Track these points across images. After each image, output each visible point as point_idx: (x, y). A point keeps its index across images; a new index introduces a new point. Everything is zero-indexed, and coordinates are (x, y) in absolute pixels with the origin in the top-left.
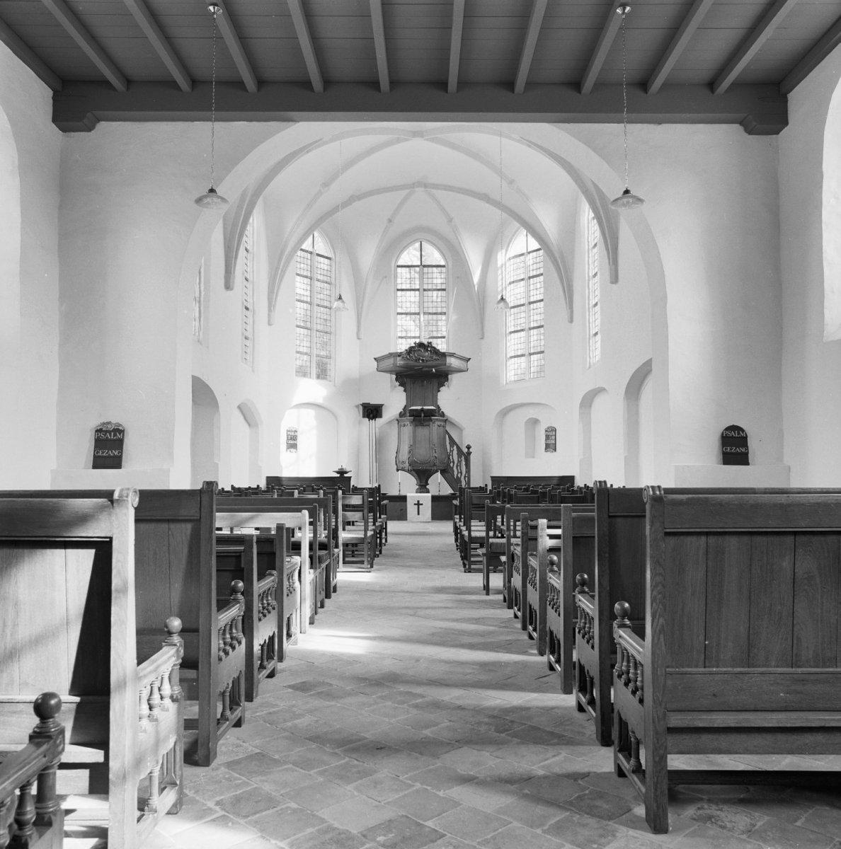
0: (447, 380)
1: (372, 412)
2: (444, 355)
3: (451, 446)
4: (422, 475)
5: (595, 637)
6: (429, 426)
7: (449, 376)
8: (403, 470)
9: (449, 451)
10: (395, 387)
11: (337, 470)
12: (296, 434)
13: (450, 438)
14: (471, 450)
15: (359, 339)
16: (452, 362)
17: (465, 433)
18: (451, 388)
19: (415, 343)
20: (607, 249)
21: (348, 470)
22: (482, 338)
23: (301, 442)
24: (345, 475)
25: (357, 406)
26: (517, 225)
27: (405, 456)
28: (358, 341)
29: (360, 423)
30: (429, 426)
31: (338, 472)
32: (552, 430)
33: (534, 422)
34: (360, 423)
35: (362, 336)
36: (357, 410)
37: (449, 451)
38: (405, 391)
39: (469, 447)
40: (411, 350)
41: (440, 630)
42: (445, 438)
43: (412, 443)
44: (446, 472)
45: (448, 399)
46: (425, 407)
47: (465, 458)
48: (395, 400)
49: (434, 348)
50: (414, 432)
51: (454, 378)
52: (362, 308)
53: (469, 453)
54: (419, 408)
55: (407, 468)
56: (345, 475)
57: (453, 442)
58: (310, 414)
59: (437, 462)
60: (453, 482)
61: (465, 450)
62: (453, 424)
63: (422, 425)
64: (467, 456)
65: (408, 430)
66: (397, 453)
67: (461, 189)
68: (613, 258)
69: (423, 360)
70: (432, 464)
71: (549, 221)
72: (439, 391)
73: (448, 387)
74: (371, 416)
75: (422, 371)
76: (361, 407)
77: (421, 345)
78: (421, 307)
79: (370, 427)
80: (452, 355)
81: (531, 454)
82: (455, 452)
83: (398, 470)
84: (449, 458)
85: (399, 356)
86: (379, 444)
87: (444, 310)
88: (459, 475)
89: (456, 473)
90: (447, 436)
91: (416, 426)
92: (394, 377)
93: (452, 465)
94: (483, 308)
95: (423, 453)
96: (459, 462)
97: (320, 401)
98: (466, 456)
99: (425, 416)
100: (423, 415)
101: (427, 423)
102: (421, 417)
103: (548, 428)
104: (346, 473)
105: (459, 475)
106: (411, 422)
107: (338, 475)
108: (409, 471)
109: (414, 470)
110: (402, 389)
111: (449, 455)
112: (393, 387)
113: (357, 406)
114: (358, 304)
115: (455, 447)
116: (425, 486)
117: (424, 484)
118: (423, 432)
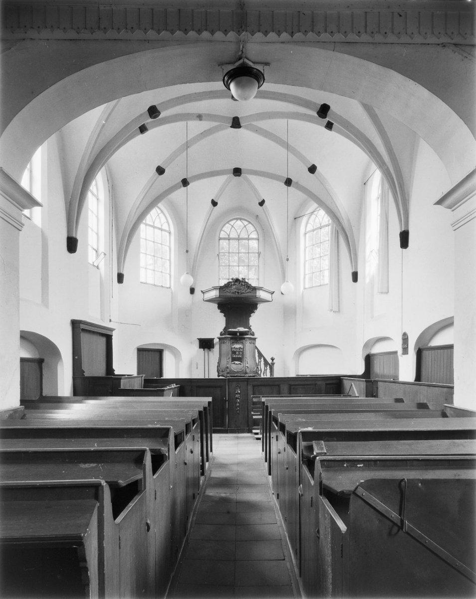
2: (255, 289)
3: (260, 358)
7: (258, 306)
9: (257, 362)
16: (261, 294)
19: (232, 279)
20: (400, 221)
23: (398, 404)
26: (315, 205)
37: (257, 362)
39: (273, 359)
40: (227, 286)
41: (373, 493)
42: (254, 353)
49: (247, 283)
51: (260, 306)
53: (273, 364)
57: (260, 355)
61: (270, 361)
66: (218, 363)
67: (178, 98)
68: (355, 135)
70: (409, 405)
71: (343, 202)
75: (237, 304)
77: (237, 280)
80: (260, 289)
82: (262, 363)
84: (258, 368)
90: (256, 350)
92: (216, 305)
96: (265, 370)
111: (258, 365)
115: (262, 359)
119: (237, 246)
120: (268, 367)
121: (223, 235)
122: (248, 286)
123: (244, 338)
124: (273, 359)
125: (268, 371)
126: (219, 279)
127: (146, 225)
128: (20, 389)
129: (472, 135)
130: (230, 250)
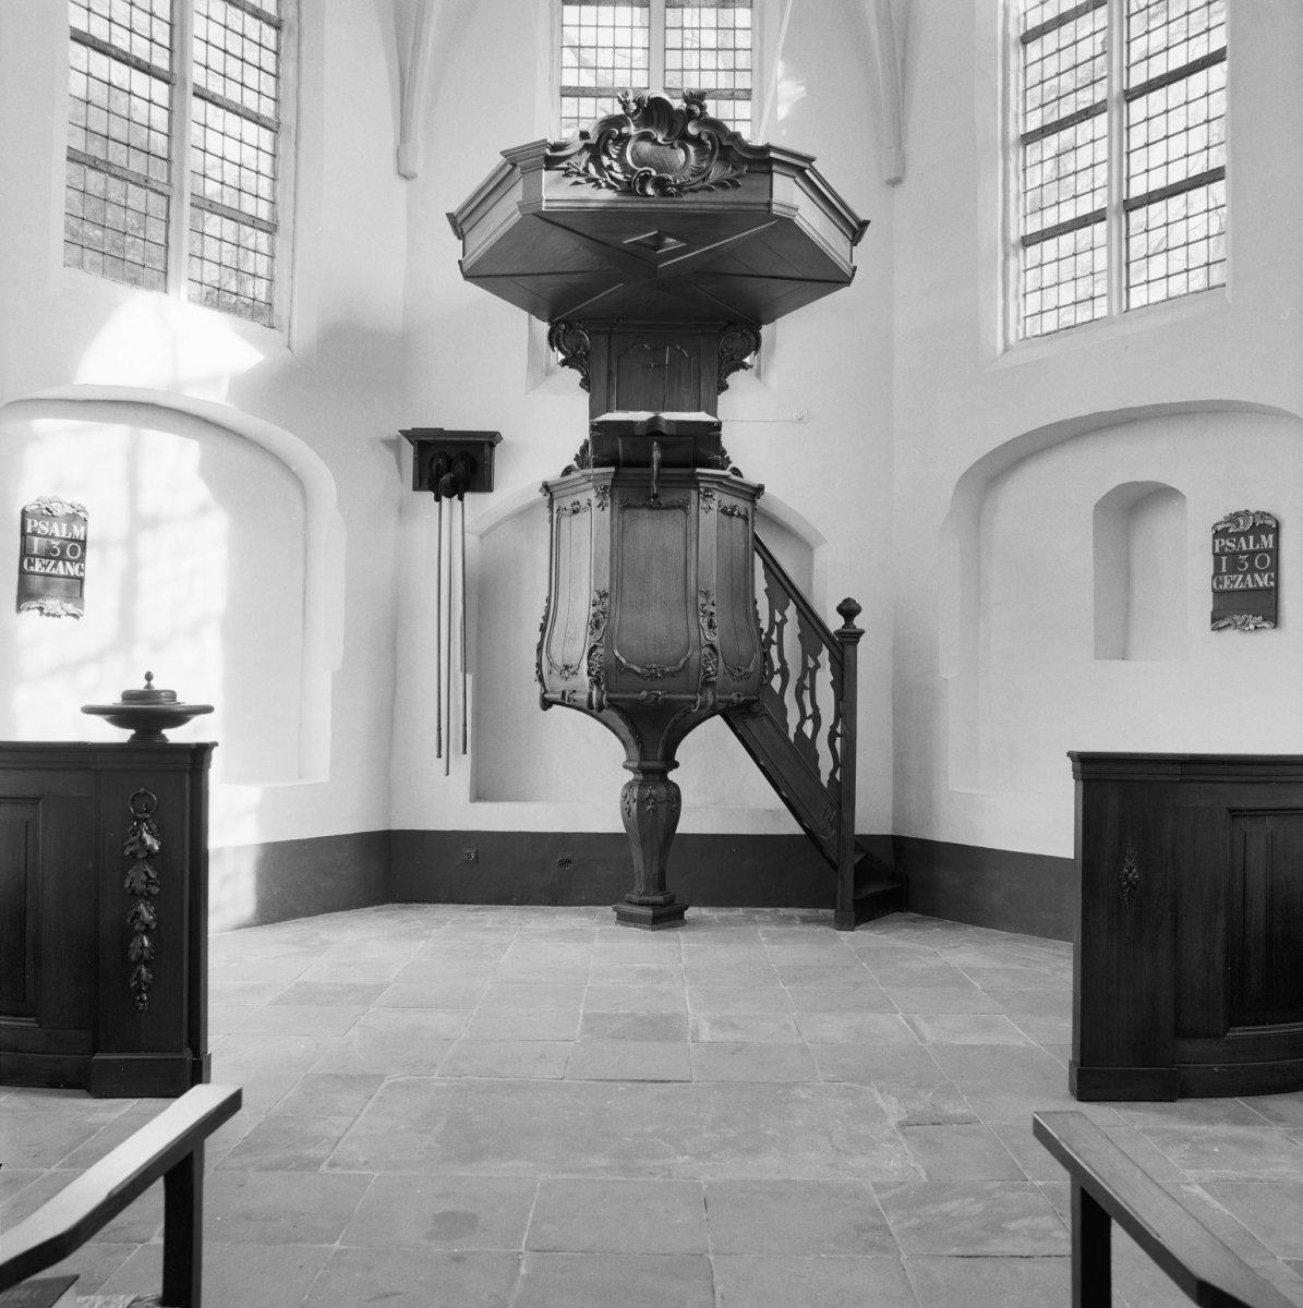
0: (755, 345)
1: (453, 464)
2: (762, 161)
4: (650, 717)
5: (188, 244)
6: (683, 507)
7: (765, 331)
8: (566, 701)
9: (765, 625)
10: (549, 372)
11: (113, 699)
12: (78, 532)
13: (772, 567)
14: (858, 622)
15: (406, 177)
17: (821, 556)
18: (773, 377)
21: (186, 699)
22: (895, 182)
24: (174, 735)
25: (392, 444)
27: (573, 643)
28: (403, 185)
29: (402, 511)
30: (683, 507)
31: (118, 716)
32: (1265, 529)
33: (1134, 505)
34: (402, 511)
35: (418, 166)
36: (390, 456)
37: (765, 625)
38: (586, 383)
39: (849, 610)
42: (748, 570)
43: (605, 585)
44: (751, 716)
45: (769, 416)
46: (667, 416)
47: (832, 657)
48: (545, 418)
50: (619, 536)
52: (416, 46)
53: (851, 637)
54: (643, 416)
55: (582, 697)
56: (174, 735)
57: (784, 588)
58: (175, 457)
59: (718, 670)
60: (784, 762)
61: (834, 623)
62: (773, 522)
63: (654, 504)
64: (844, 646)
65: (590, 528)
66: (543, 629)
69: (660, 184)
72: (723, 387)
73: (758, 375)
74: (446, 478)
75: (665, 271)
76: (409, 450)
77: (653, 112)
78: (657, 68)
79: (442, 528)
80: (800, 167)
81: (1117, 633)
82: (791, 631)
83: (546, 704)
84: (766, 656)
85: (551, 163)
86: (480, 598)
87: (743, 82)
88: (808, 728)
89: (793, 718)
90: (758, 562)
91: (626, 506)
93: (776, 683)
94: (904, 61)
95: (658, 629)
96: (809, 672)
97: (214, 400)
98: (840, 647)
99: (663, 464)
100: (656, 455)
101: (676, 496)
102: (655, 467)
103: (1234, 518)
104: (179, 718)
105: (808, 728)
106: (602, 494)
107: (122, 735)
108: (589, 709)
109: (614, 704)
110: (575, 376)
112: (542, 373)
113: (392, 444)
114: (401, 50)
116: (664, 773)
117: (658, 765)
118: (655, 531)
119: (1116, 1150)
120: (825, 654)
121: (1225, 210)
122: (723, 145)
123: (693, 482)
124: (849, 610)
125: (825, 677)
126: (649, 28)
127: (133, 457)
128: (163, 1146)
129: (171, 1107)
130: (152, 219)
